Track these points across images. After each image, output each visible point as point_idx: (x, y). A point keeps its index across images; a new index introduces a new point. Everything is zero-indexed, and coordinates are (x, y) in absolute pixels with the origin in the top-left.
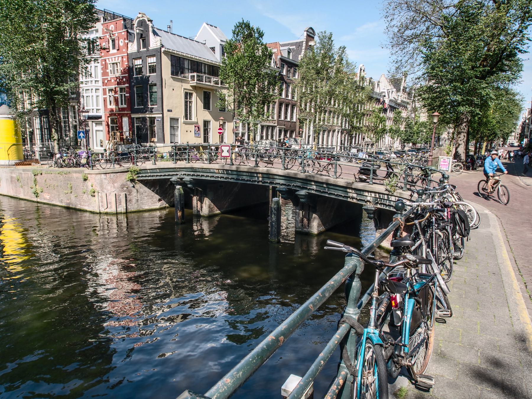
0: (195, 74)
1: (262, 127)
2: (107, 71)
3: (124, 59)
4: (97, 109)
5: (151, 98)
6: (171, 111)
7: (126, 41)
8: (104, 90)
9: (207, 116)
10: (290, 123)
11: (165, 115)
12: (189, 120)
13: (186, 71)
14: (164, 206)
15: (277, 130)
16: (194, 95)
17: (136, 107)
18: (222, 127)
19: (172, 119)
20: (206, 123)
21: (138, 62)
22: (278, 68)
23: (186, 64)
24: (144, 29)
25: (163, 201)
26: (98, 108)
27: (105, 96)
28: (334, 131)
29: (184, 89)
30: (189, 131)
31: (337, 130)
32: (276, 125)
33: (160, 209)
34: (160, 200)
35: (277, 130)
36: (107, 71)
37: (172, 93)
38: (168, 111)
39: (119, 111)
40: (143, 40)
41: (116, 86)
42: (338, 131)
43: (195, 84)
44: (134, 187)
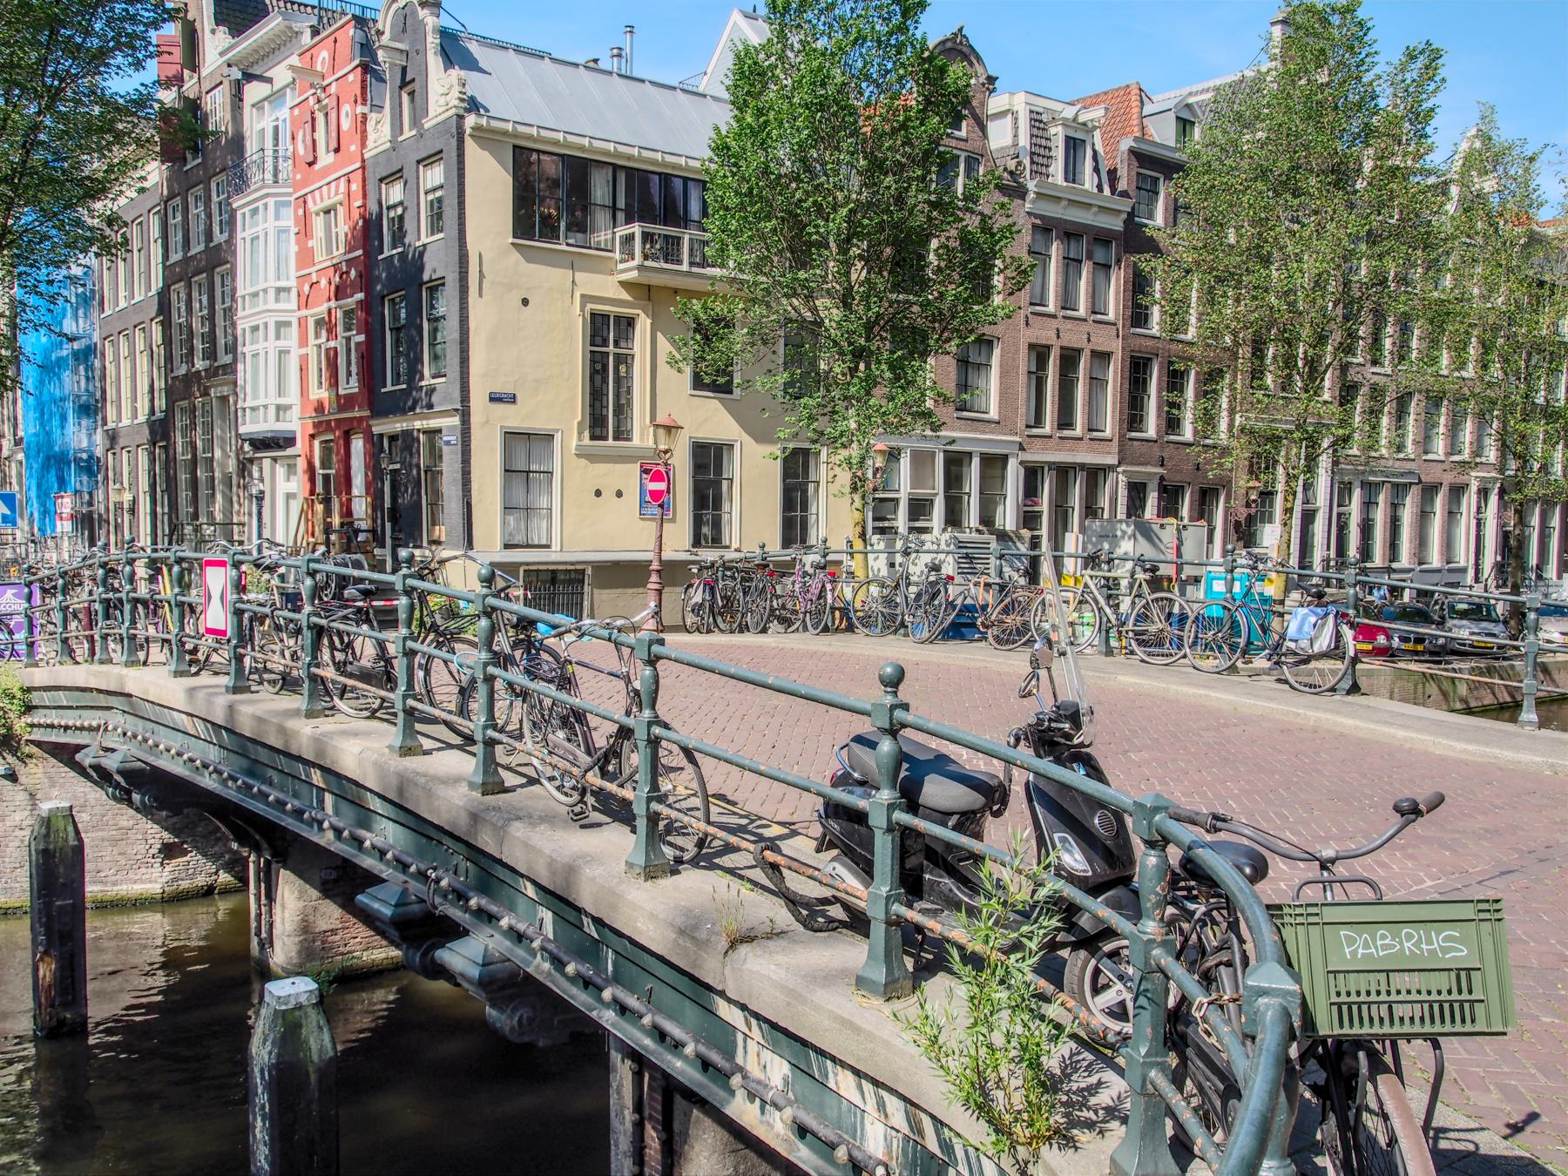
0: (636, 229)
1: (1032, 475)
2: (310, 244)
3: (354, 187)
4: (279, 408)
5: (432, 345)
6: (512, 399)
7: (360, 109)
8: (302, 322)
9: (711, 419)
10: (1155, 448)
11: (476, 419)
12: (611, 442)
13: (601, 217)
14: (201, 881)
15: (1115, 491)
16: (643, 324)
17: (389, 388)
18: (796, 469)
19: (511, 436)
20: (709, 461)
21: (395, 193)
22: (1125, 194)
23: (600, 190)
24: (412, 43)
25: (193, 858)
26: (282, 401)
27: (304, 351)
28: (1457, 491)
29: (586, 299)
30: (608, 494)
31: (1474, 487)
32: (1112, 460)
33: (173, 900)
34: (169, 852)
35: (1115, 491)
36: (310, 244)
37: (520, 324)
38: (495, 399)
39: (341, 409)
40: (411, 94)
41: (333, 304)
42: (1484, 493)
43: (635, 274)
44: (12, 777)
